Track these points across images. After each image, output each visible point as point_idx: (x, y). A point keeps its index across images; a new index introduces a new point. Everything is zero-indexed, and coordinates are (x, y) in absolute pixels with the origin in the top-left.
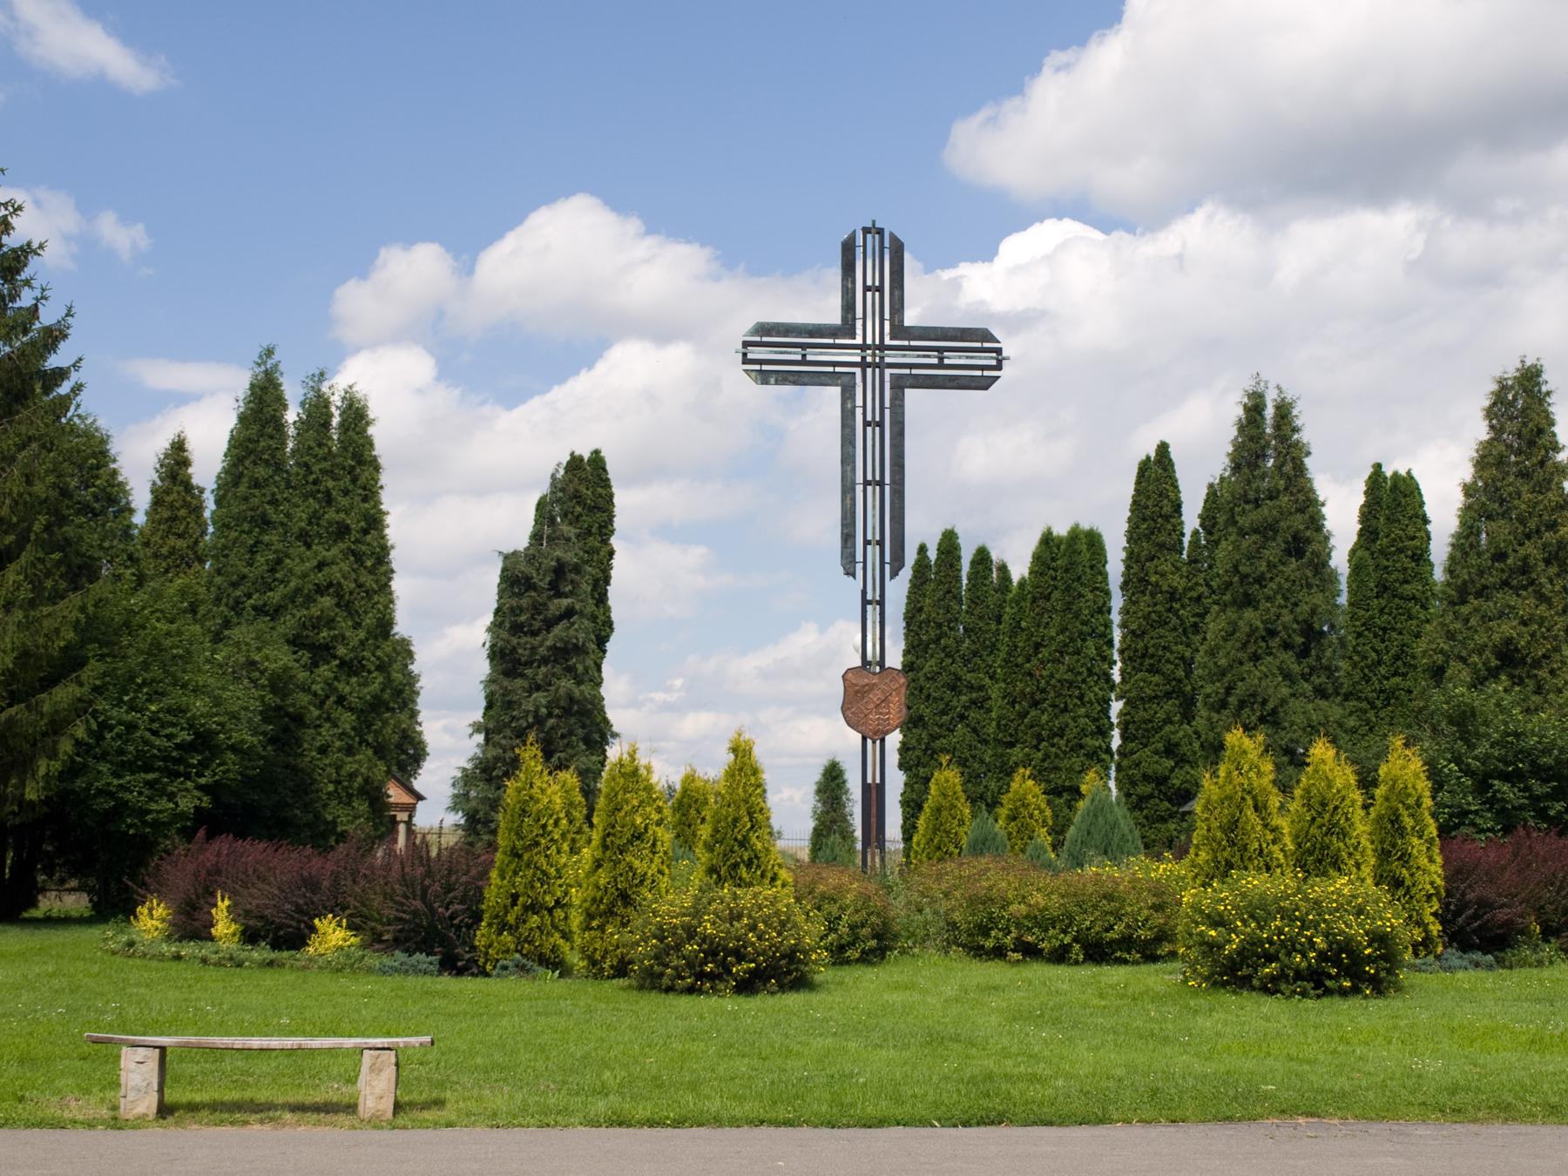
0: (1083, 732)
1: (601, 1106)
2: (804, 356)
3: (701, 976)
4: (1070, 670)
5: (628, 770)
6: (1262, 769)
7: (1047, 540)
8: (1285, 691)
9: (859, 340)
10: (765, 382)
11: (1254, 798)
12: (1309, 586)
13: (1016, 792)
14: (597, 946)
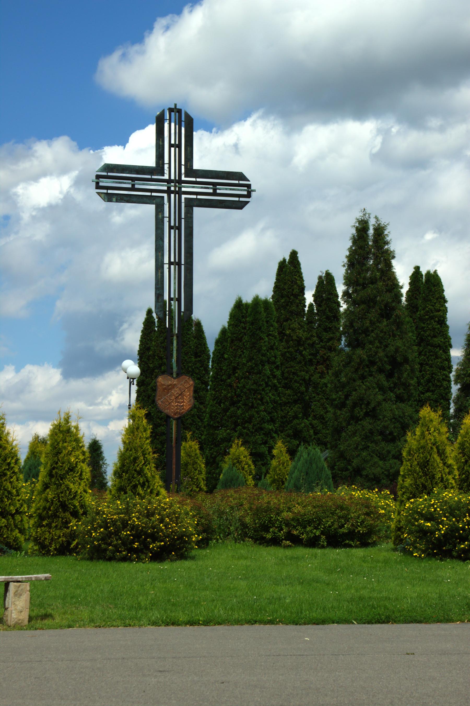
0: (263, 420)
1: (155, 615)
2: (133, 185)
3: (131, 550)
4: (255, 383)
5: (65, 429)
6: (441, 431)
7: (239, 305)
8: (380, 397)
9: (166, 177)
10: (110, 200)
11: (437, 448)
12: (394, 336)
13: (234, 454)
14: (47, 536)
